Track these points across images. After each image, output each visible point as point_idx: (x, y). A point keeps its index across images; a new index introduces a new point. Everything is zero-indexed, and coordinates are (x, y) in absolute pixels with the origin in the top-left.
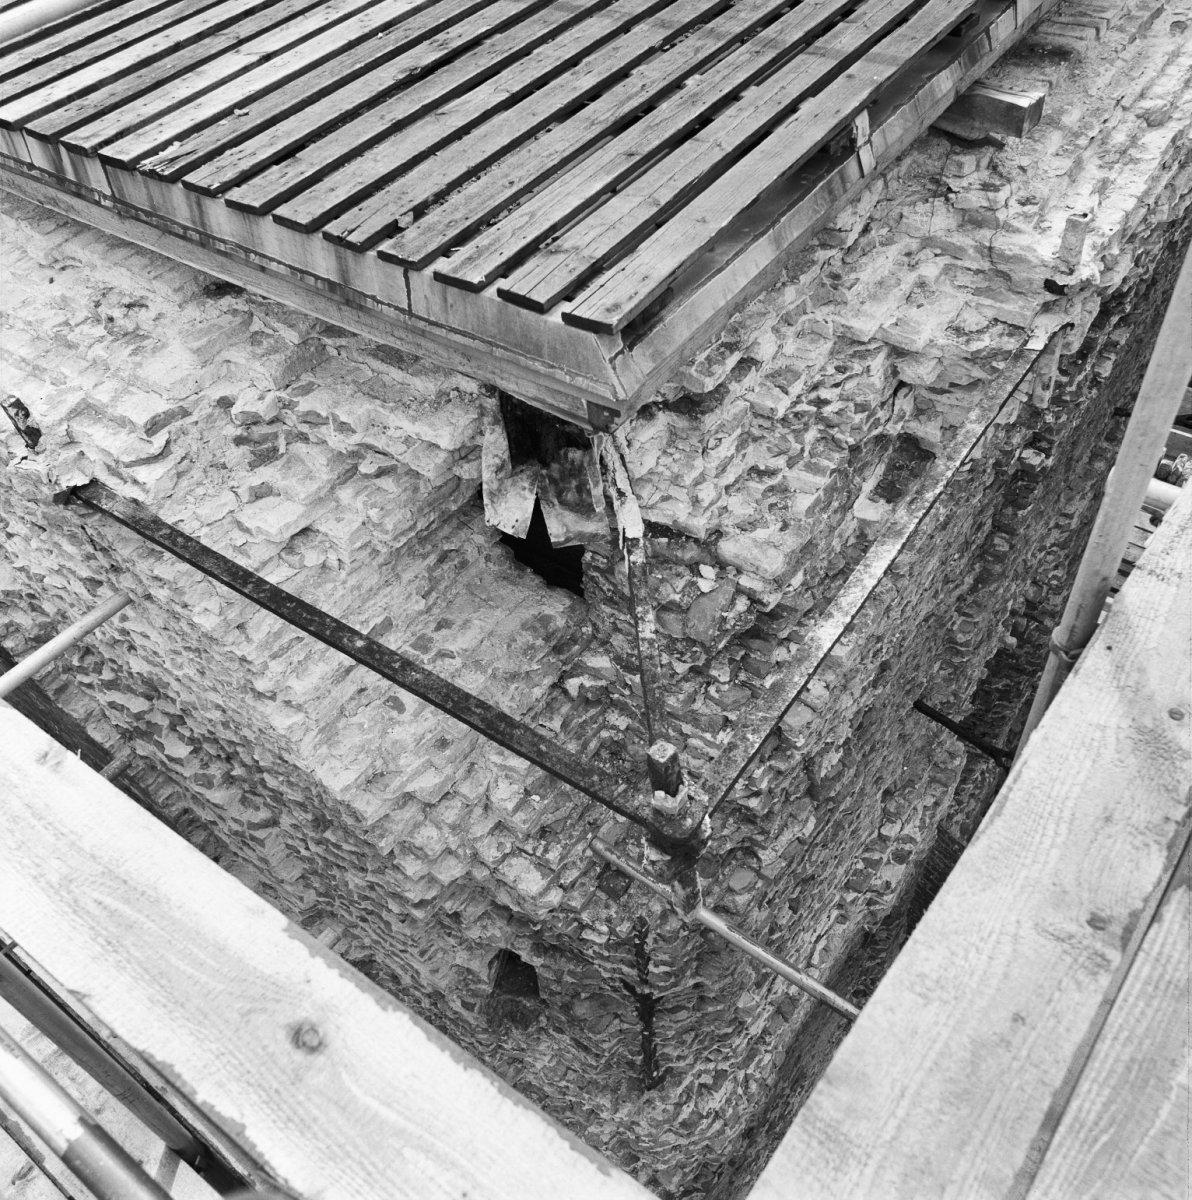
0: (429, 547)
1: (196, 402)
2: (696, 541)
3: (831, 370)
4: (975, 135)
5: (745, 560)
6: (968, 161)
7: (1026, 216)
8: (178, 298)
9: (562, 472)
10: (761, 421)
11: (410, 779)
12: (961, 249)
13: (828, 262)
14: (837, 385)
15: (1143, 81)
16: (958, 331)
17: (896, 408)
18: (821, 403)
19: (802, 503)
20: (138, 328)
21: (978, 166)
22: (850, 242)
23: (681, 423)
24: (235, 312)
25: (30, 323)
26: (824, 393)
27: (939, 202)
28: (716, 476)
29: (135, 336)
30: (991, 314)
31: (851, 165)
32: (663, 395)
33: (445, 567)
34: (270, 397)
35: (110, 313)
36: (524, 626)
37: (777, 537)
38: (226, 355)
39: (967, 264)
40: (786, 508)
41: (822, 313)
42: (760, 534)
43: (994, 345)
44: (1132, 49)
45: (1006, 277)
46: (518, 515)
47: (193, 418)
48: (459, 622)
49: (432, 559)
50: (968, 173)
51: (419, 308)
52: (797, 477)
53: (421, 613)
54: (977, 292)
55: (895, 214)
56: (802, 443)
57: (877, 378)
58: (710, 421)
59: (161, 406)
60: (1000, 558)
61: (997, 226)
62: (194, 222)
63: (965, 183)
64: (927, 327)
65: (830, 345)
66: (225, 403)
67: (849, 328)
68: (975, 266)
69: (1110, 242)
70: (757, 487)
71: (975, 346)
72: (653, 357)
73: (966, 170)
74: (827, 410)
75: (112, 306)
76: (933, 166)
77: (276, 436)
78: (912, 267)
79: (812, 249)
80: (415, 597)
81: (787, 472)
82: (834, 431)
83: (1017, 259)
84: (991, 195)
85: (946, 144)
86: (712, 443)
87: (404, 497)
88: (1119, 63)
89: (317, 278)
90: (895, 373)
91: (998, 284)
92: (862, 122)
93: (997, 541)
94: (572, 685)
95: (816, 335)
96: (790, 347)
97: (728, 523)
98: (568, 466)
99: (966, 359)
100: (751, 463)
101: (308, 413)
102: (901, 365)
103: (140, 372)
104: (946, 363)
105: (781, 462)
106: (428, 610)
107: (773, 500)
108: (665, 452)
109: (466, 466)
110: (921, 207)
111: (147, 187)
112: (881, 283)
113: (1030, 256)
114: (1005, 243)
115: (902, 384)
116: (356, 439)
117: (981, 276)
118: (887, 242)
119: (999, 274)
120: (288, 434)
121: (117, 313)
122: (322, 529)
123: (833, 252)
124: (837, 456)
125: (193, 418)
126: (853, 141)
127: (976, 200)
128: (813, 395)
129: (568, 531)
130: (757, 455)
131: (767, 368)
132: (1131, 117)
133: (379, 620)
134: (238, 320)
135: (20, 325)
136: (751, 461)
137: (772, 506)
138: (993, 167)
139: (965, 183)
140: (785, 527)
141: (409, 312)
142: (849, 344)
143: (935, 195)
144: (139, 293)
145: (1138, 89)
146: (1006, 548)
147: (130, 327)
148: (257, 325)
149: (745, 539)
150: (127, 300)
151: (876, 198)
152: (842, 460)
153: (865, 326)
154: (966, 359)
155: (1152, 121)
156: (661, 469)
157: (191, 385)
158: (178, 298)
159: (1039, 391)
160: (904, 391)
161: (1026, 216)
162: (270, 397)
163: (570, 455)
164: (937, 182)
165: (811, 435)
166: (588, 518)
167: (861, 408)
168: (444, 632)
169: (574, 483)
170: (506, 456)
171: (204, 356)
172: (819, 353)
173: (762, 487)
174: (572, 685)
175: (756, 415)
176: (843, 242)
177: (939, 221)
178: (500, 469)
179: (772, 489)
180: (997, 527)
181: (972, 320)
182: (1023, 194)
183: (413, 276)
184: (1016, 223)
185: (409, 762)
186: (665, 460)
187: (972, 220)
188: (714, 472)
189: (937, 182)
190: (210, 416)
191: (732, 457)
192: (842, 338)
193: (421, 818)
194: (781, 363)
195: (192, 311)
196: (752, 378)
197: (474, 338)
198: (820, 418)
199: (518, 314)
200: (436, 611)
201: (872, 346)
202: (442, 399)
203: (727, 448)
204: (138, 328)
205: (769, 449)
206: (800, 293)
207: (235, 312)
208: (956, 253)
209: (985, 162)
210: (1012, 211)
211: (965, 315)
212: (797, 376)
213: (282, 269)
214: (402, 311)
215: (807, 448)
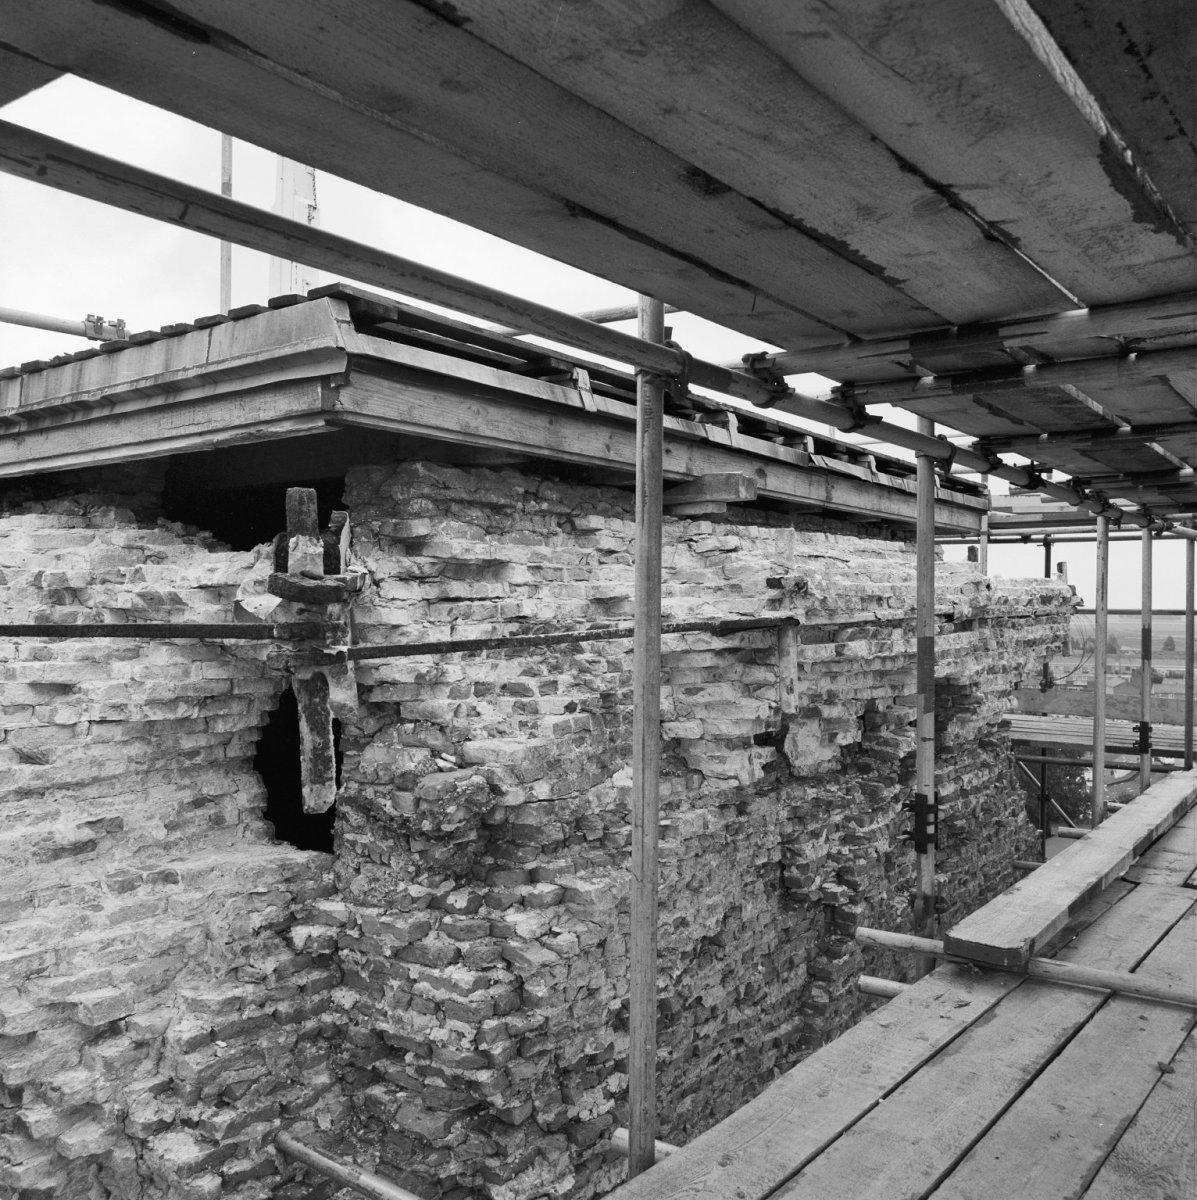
0: (187, 781)
11: (78, 986)
27: (683, 547)
33: (199, 812)
49: (187, 796)
60: (820, 1010)
68: (713, 585)
80: (156, 821)
81: (537, 697)
87: (172, 671)
93: (815, 992)
94: (299, 934)
97: (477, 725)
117: (719, 593)
122: (84, 686)
146: (825, 999)
159: (785, 696)
174: (299, 934)
180: (813, 975)
185: (86, 966)
193: (75, 1059)
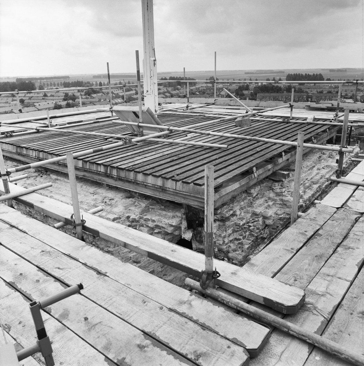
1: (123, 216)
2: (224, 252)
3: (251, 219)
4: (277, 179)
5: (234, 257)
6: (277, 184)
7: (289, 194)
8: (121, 198)
9: (197, 233)
10: (237, 227)
12: (276, 200)
13: (250, 200)
14: (252, 223)
15: (311, 176)
16: (277, 214)
17: (265, 231)
18: (250, 226)
19: (246, 246)
20: (111, 204)
21: (278, 185)
22: (254, 196)
23: (221, 224)
24: (132, 201)
25: (88, 203)
26: (250, 224)
27: (271, 191)
28: (228, 237)
29: (111, 205)
30: (283, 211)
31: (253, 175)
32: (218, 218)
34: (138, 216)
35: (106, 201)
36: (183, 276)
37: (241, 253)
38: (130, 208)
39: (278, 203)
40: (242, 248)
41: (249, 209)
42: (237, 252)
43: (284, 217)
44: (309, 172)
45: (286, 205)
46: (189, 236)
47: (122, 220)
48: (169, 274)
50: (277, 187)
51: (178, 189)
52: (245, 241)
53: (160, 272)
54: (280, 208)
55: (263, 193)
56: (246, 234)
57: (261, 222)
58: (227, 223)
59: (116, 216)
61: (283, 196)
62: (134, 178)
63: (276, 188)
64: (270, 212)
65: (251, 214)
66: (128, 217)
67: (254, 211)
68: (279, 203)
69: (306, 201)
70: (236, 242)
71: (280, 216)
72: (219, 195)
73: (276, 185)
74: (251, 228)
75: (107, 200)
76: (270, 185)
77: (137, 225)
78: (267, 203)
79: (247, 197)
80: (159, 267)
82: (253, 233)
83: (287, 201)
84: (281, 190)
85: (272, 181)
86: (227, 229)
88: (307, 173)
89: (158, 186)
90: (264, 222)
91: (284, 206)
92: (254, 169)
95: (248, 212)
96: (243, 214)
98: (198, 231)
99: (279, 219)
100: (235, 237)
101: (146, 219)
102: (266, 220)
103: (112, 210)
104: (275, 221)
105: (241, 237)
106: (162, 272)
107: (240, 246)
108: (218, 230)
109: (177, 232)
110: (268, 192)
111: (125, 173)
112: (260, 205)
113: (290, 200)
114: (284, 198)
115: (267, 225)
116: (155, 224)
118: (262, 198)
119: (284, 204)
120: (140, 225)
121: (107, 201)
123: (251, 198)
124: (253, 238)
125: (122, 220)
126: (253, 171)
127: (278, 191)
128: (248, 225)
129: (197, 247)
130: (236, 235)
131: (238, 217)
132: (310, 182)
133: (152, 270)
134: (133, 202)
135: (86, 203)
136: (235, 236)
137: (240, 247)
138: (282, 186)
139: (276, 188)
140: (242, 251)
141: (176, 190)
142: (255, 214)
143: (270, 190)
144: (113, 197)
145: (311, 177)
147: (110, 204)
148: (136, 204)
149: (234, 253)
150: (110, 199)
151: (259, 189)
152: (254, 239)
153: (258, 210)
154: (279, 219)
155: (314, 183)
156: (217, 233)
157: (122, 213)
158: (121, 198)
160: (267, 227)
161: (289, 194)
162: (138, 216)
163: (199, 229)
164: (271, 188)
165: (247, 233)
166: (201, 244)
167: (258, 229)
168: (165, 276)
169: (199, 236)
170: (187, 226)
171: (126, 208)
172: (249, 216)
173: (237, 242)
175: (236, 225)
176: (253, 196)
177: (272, 195)
178: (185, 228)
179: (239, 243)
181: (279, 212)
182: (288, 191)
183: (178, 183)
184: (287, 195)
186: (217, 232)
187: (278, 194)
188: (228, 236)
189: (271, 188)
190: (125, 220)
191: (231, 233)
192: (253, 213)
194: (241, 217)
195: (124, 200)
196: (235, 218)
197: (187, 193)
198: (249, 230)
199: (197, 187)
200: (163, 272)
201: (259, 216)
202: (174, 217)
203: (230, 231)
204: (111, 204)
205: (239, 234)
206: (244, 204)
207: (132, 201)
208: (275, 200)
209: (280, 185)
210: (286, 193)
211: (278, 212)
212: (244, 219)
213: (151, 185)
214: (174, 190)
215: (247, 236)
